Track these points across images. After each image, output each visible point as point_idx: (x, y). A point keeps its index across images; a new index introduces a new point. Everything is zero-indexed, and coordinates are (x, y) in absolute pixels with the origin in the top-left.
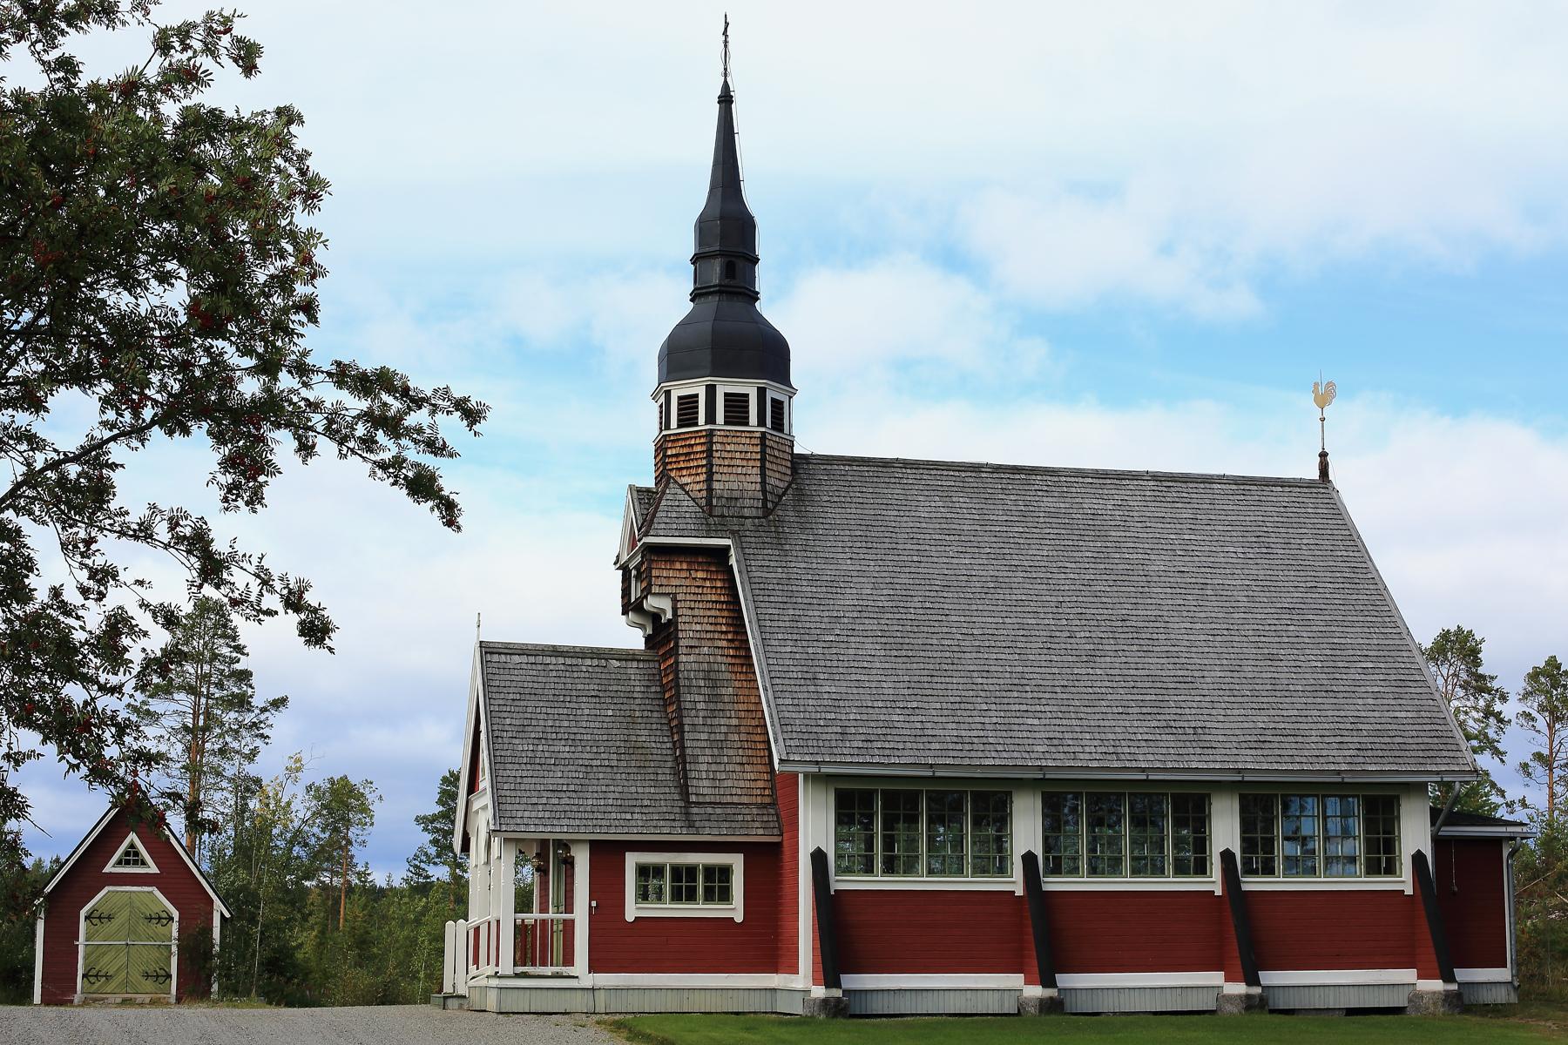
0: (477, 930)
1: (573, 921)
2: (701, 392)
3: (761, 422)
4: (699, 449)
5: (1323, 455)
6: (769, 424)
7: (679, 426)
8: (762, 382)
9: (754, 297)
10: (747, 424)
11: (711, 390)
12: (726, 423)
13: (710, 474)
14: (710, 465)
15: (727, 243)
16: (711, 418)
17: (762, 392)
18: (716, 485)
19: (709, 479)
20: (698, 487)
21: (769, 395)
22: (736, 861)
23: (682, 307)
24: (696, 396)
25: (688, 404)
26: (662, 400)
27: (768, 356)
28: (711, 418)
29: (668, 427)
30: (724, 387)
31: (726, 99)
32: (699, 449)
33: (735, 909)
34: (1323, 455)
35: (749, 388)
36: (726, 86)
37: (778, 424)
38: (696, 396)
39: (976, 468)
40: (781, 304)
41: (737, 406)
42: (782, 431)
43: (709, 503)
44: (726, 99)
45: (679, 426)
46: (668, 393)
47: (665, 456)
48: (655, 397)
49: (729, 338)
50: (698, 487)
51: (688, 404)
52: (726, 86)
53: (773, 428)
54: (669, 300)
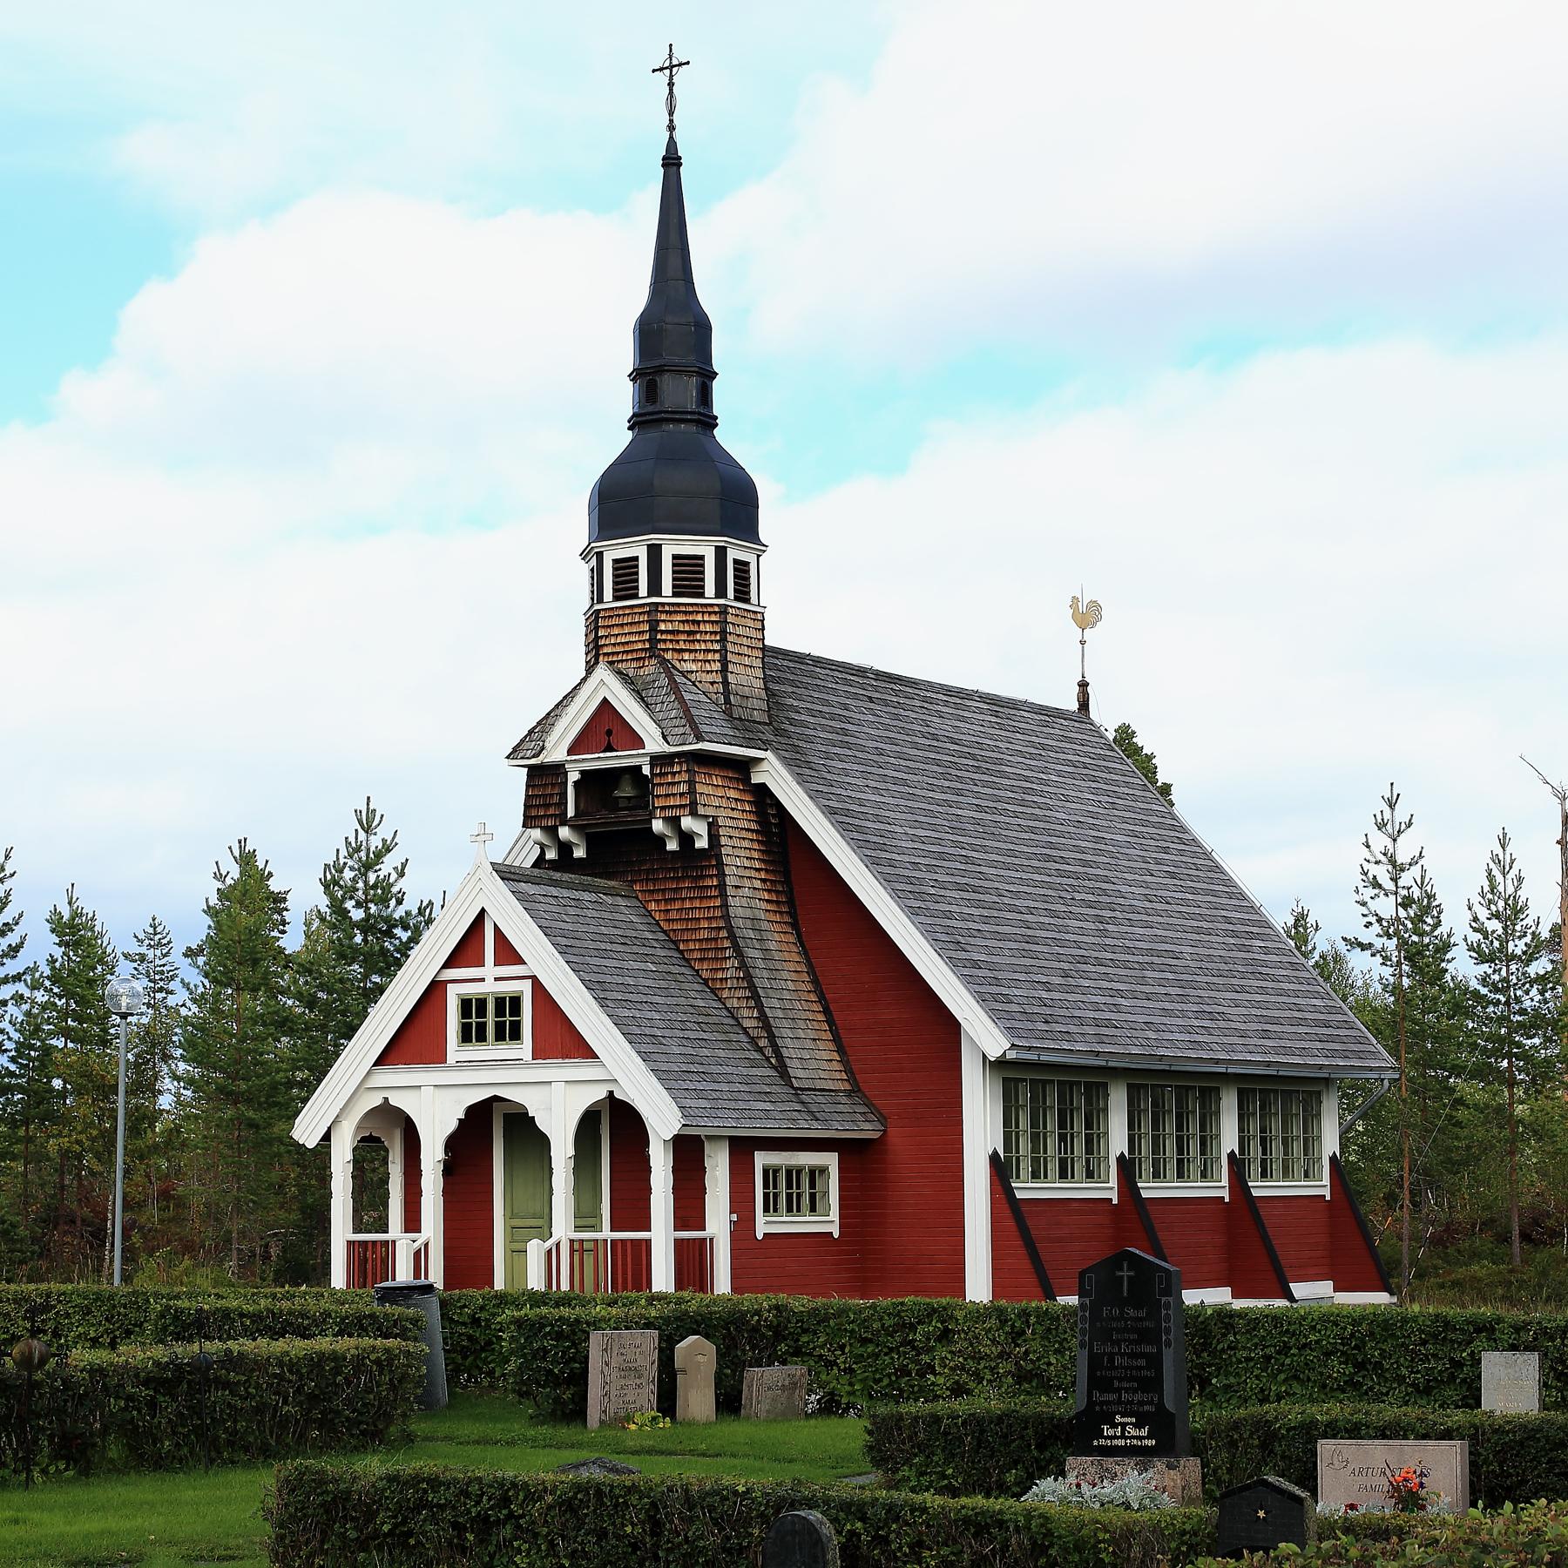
0: (558, 1245)
1: (648, 1242)
2: (642, 553)
3: (721, 591)
4: (708, 628)
5: (1083, 685)
6: (731, 593)
7: (616, 598)
8: (721, 540)
9: (710, 423)
10: (702, 595)
11: (655, 552)
12: (675, 595)
13: (724, 663)
14: (723, 652)
15: (674, 348)
16: (654, 588)
17: (721, 553)
18: (731, 678)
19: (724, 670)
20: (710, 678)
21: (732, 554)
22: (831, 1160)
23: (621, 438)
24: (636, 559)
25: (626, 569)
26: (594, 562)
27: (733, 506)
28: (654, 588)
29: (600, 600)
30: (673, 547)
31: (672, 161)
32: (708, 628)
33: (829, 1222)
34: (1083, 685)
35: (704, 548)
36: (672, 144)
37: (743, 594)
38: (636, 559)
39: (861, 671)
40: (741, 430)
41: (689, 570)
42: (747, 601)
43: (728, 701)
44: (672, 161)
45: (616, 598)
46: (600, 555)
47: (597, 638)
48: (584, 555)
49: (674, 475)
50: (710, 678)
51: (626, 569)
52: (672, 144)
53: (737, 599)
54: (605, 430)
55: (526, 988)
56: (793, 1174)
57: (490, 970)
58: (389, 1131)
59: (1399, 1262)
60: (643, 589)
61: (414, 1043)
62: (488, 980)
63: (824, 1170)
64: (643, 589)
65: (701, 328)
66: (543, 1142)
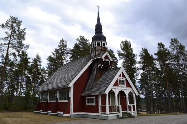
1: (106, 106)
2: (95, 43)
9: (102, 33)
17: (102, 42)
21: (103, 42)
27: (104, 38)
31: (98, 14)
36: (98, 12)
40: (105, 33)
41: (99, 44)
44: (98, 14)
52: (98, 12)
55: (125, 80)
56: (91, 99)
57: (122, 77)
58: (112, 93)
59: (117, 116)
60: (101, 45)
61: (116, 84)
62: (122, 79)
63: (94, 98)
64: (101, 45)
65: (101, 26)
66: (125, 95)
